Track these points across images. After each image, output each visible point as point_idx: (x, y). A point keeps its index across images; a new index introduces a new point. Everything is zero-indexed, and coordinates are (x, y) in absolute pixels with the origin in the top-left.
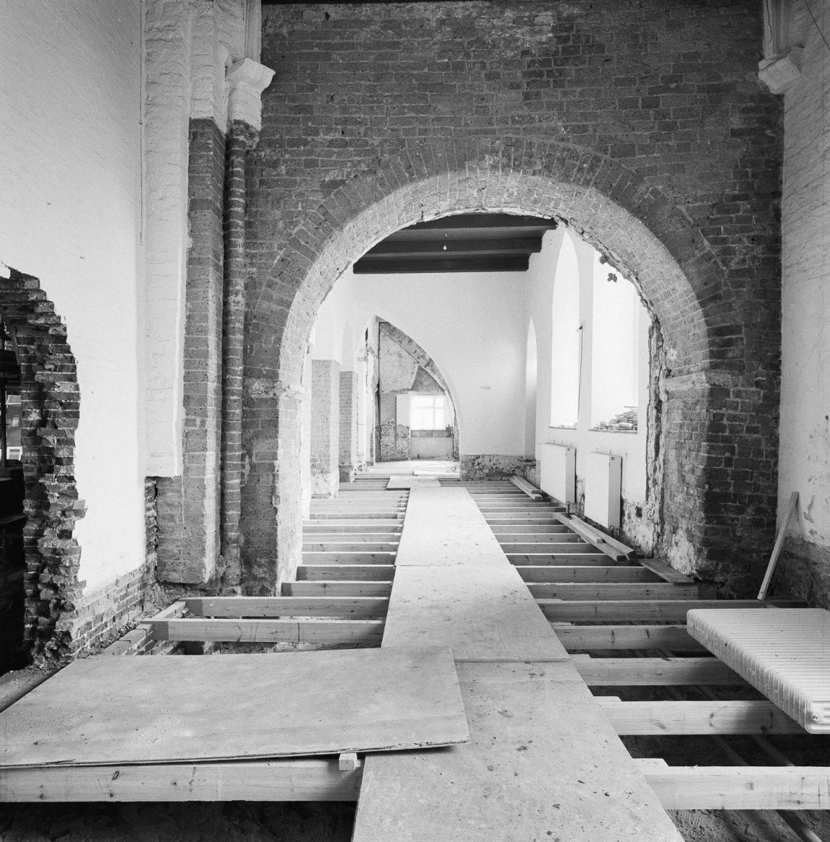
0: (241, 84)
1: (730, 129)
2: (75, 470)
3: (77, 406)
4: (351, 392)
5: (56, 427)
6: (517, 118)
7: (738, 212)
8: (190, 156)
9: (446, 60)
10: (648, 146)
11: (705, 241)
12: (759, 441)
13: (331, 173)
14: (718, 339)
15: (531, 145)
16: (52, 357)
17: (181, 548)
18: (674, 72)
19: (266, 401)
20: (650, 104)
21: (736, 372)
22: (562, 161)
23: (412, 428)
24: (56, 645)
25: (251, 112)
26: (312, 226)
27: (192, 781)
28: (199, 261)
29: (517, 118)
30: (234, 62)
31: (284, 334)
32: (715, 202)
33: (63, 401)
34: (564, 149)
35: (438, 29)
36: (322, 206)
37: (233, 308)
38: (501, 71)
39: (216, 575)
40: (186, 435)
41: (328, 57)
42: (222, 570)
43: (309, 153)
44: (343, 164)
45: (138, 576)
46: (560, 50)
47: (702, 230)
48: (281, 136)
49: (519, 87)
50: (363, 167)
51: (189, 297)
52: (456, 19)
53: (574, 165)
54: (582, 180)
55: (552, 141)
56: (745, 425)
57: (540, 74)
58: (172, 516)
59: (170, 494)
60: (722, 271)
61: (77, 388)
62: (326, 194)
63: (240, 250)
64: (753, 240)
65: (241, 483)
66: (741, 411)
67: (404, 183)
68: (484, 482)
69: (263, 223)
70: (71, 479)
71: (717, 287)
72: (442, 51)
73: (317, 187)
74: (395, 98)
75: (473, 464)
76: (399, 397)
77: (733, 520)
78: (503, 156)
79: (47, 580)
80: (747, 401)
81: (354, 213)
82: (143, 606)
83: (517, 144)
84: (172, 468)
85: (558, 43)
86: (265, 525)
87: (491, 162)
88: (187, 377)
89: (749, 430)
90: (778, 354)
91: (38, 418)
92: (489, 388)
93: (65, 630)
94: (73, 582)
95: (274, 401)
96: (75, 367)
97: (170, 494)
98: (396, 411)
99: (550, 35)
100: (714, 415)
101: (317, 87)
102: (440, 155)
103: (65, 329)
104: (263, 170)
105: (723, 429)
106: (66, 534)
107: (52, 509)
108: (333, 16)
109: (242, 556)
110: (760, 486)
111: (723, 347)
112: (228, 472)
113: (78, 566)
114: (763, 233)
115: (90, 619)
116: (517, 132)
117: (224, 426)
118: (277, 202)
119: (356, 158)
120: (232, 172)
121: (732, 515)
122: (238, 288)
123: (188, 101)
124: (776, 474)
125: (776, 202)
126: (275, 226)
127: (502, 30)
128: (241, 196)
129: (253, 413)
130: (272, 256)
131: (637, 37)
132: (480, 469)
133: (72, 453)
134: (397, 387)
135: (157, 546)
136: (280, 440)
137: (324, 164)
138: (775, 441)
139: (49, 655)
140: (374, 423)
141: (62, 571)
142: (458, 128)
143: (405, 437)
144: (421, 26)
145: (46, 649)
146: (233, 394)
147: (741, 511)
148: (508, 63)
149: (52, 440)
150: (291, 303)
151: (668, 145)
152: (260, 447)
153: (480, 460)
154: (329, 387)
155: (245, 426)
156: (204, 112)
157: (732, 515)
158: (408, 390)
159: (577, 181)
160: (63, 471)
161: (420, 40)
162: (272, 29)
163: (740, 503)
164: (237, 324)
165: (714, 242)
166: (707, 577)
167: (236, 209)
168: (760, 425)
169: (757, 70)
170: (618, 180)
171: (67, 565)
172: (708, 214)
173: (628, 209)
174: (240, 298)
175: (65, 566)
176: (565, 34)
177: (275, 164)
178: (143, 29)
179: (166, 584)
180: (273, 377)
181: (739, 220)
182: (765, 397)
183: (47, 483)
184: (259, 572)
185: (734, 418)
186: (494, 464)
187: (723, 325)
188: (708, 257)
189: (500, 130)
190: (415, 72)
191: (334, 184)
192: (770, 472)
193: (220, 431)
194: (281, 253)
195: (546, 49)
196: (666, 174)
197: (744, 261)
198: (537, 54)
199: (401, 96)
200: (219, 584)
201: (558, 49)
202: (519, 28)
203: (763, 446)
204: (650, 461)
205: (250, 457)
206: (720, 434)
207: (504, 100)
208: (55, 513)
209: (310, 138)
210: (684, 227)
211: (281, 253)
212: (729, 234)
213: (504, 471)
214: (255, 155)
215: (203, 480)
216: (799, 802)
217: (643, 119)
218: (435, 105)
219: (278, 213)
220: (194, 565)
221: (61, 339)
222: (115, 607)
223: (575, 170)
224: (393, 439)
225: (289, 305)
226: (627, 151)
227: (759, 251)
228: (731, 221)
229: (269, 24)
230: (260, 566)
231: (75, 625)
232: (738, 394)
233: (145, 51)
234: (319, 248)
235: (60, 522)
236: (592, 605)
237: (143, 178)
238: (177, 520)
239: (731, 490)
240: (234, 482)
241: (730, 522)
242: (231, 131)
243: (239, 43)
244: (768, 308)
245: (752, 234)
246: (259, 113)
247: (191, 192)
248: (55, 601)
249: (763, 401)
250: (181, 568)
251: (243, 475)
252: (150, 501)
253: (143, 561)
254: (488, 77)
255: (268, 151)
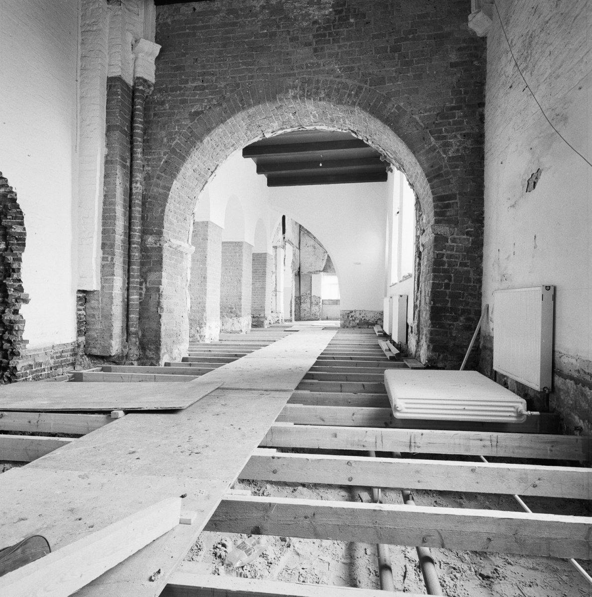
0: (140, 55)
1: (449, 62)
2: (22, 275)
3: (24, 240)
4: (266, 267)
5: (12, 251)
6: (309, 65)
7: (455, 117)
8: (107, 99)
9: (266, 31)
10: (394, 77)
11: (432, 138)
12: (468, 272)
13: (195, 107)
14: (440, 204)
15: (318, 81)
16: (10, 211)
17: (99, 334)
18: (411, 27)
19: (155, 248)
20: (395, 49)
21: (453, 226)
22: (338, 90)
23: (323, 298)
24: (10, 374)
25: (148, 71)
26: (184, 140)
27: (38, 421)
28: (112, 162)
29: (309, 65)
30: (136, 41)
31: (167, 207)
32: (438, 112)
33: (17, 237)
34: (339, 83)
35: (261, 12)
36: (190, 127)
37: (134, 191)
38: (300, 35)
39: (122, 353)
40: (103, 266)
41: (194, 35)
42: (126, 351)
43: (183, 95)
44: (202, 101)
45: (70, 347)
46: (337, 19)
47: (430, 131)
48: (166, 86)
49: (310, 44)
50: (215, 102)
51: (106, 184)
52: (272, 5)
53: (345, 93)
54: (350, 102)
55: (332, 78)
56: (459, 261)
57: (325, 35)
58: (94, 315)
59: (93, 302)
60: (443, 158)
61: (24, 229)
62: (192, 120)
63: (139, 156)
64: (464, 136)
65: (140, 299)
66: (456, 251)
67: (239, 111)
68: (355, 329)
69: (155, 140)
70: (20, 281)
71: (440, 168)
72: (263, 26)
73: (187, 116)
74: (234, 57)
75: (348, 316)
76: (314, 276)
77: (450, 325)
78: (300, 89)
79: (6, 338)
80: (461, 245)
81: (209, 131)
82: (74, 367)
83: (309, 82)
84: (93, 284)
85: (335, 15)
86: (154, 326)
87: (293, 94)
88: (104, 232)
89: (462, 264)
90: (482, 213)
91: (4, 247)
92: (360, 264)
93: (14, 366)
94: (20, 339)
95: (160, 249)
96: (23, 217)
97: (93, 302)
98: (311, 286)
99: (331, 10)
100: (437, 255)
101: (187, 54)
102: (261, 91)
103: (16, 195)
104: (155, 107)
105: (443, 264)
106: (16, 312)
107: (10, 298)
108: (198, 9)
109: (140, 344)
110: (469, 303)
111: (443, 209)
112: (131, 291)
113: (23, 331)
114: (472, 131)
115: (32, 363)
116: (309, 73)
117: (129, 262)
118: (163, 127)
119: (210, 96)
120: (135, 109)
121: (449, 322)
122: (137, 179)
123: (107, 66)
124: (481, 294)
125: (481, 109)
126: (162, 141)
127: (300, 9)
128: (141, 123)
129: (148, 257)
130: (160, 159)
131: (387, 6)
132: (353, 320)
133: (20, 266)
134: (312, 269)
135: (85, 333)
136: (163, 274)
137: (192, 101)
138: (479, 272)
139: (6, 380)
140: (293, 292)
141: (14, 333)
142: (272, 74)
143: (317, 304)
144: (251, 11)
145: (4, 376)
146: (134, 244)
147: (456, 319)
148: (303, 30)
149: (10, 258)
150: (171, 188)
151: (408, 76)
152: (152, 277)
153: (352, 314)
154: (242, 259)
155: (142, 264)
156: (116, 72)
157: (449, 322)
158: (320, 271)
159: (347, 103)
160: (15, 276)
161: (249, 19)
162: (162, 20)
163: (455, 314)
164: (137, 201)
165: (437, 139)
166: (433, 364)
167: (137, 131)
168: (469, 261)
169: (467, 21)
170: (374, 101)
171: (17, 329)
172: (434, 120)
173: (380, 120)
174: (138, 185)
175: (16, 330)
176: (340, 8)
177: (163, 103)
178: (80, 25)
179: (92, 356)
180: (160, 234)
181: (455, 123)
182: (473, 242)
183: (7, 283)
184: (150, 354)
185: (451, 256)
186: (363, 317)
187: (443, 194)
188: (433, 149)
189: (299, 73)
190: (247, 40)
191: (197, 113)
192: (476, 293)
193: (127, 266)
194: (165, 157)
195: (328, 18)
196: (406, 95)
197: (458, 150)
198: (322, 23)
199: (238, 56)
200: (120, 360)
201: (336, 18)
202: (312, 7)
203: (472, 275)
204: (415, 293)
205: (146, 283)
206: (441, 267)
207: (302, 54)
208: (11, 300)
209: (183, 86)
210: (418, 129)
211: (165, 157)
212: (448, 132)
213: (370, 321)
214: (151, 98)
215: (112, 293)
216: (364, 446)
217: (391, 60)
218: (258, 60)
219: (164, 133)
220: (106, 345)
221: (14, 200)
222: (52, 362)
223: (346, 96)
224: (309, 306)
225: (169, 189)
226: (381, 81)
227: (469, 143)
228: (449, 124)
229: (160, 17)
230: (150, 350)
231: (20, 364)
232: (454, 240)
233: (80, 38)
234: (188, 153)
235: (14, 305)
236: (345, 375)
237: (78, 113)
238: (97, 317)
239: (449, 305)
240: (135, 297)
241: (448, 326)
242: (135, 83)
243: (139, 29)
244: (475, 182)
245: (464, 132)
246: (153, 72)
247: (107, 121)
248: (10, 350)
249: (472, 244)
250: (98, 346)
251: (141, 294)
252: (81, 305)
253: (75, 339)
254: (291, 40)
255: (159, 95)
